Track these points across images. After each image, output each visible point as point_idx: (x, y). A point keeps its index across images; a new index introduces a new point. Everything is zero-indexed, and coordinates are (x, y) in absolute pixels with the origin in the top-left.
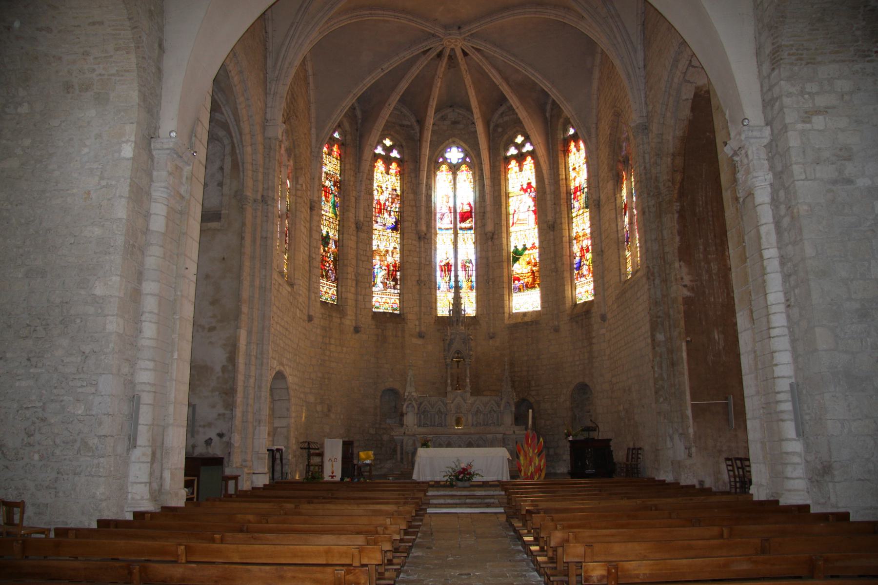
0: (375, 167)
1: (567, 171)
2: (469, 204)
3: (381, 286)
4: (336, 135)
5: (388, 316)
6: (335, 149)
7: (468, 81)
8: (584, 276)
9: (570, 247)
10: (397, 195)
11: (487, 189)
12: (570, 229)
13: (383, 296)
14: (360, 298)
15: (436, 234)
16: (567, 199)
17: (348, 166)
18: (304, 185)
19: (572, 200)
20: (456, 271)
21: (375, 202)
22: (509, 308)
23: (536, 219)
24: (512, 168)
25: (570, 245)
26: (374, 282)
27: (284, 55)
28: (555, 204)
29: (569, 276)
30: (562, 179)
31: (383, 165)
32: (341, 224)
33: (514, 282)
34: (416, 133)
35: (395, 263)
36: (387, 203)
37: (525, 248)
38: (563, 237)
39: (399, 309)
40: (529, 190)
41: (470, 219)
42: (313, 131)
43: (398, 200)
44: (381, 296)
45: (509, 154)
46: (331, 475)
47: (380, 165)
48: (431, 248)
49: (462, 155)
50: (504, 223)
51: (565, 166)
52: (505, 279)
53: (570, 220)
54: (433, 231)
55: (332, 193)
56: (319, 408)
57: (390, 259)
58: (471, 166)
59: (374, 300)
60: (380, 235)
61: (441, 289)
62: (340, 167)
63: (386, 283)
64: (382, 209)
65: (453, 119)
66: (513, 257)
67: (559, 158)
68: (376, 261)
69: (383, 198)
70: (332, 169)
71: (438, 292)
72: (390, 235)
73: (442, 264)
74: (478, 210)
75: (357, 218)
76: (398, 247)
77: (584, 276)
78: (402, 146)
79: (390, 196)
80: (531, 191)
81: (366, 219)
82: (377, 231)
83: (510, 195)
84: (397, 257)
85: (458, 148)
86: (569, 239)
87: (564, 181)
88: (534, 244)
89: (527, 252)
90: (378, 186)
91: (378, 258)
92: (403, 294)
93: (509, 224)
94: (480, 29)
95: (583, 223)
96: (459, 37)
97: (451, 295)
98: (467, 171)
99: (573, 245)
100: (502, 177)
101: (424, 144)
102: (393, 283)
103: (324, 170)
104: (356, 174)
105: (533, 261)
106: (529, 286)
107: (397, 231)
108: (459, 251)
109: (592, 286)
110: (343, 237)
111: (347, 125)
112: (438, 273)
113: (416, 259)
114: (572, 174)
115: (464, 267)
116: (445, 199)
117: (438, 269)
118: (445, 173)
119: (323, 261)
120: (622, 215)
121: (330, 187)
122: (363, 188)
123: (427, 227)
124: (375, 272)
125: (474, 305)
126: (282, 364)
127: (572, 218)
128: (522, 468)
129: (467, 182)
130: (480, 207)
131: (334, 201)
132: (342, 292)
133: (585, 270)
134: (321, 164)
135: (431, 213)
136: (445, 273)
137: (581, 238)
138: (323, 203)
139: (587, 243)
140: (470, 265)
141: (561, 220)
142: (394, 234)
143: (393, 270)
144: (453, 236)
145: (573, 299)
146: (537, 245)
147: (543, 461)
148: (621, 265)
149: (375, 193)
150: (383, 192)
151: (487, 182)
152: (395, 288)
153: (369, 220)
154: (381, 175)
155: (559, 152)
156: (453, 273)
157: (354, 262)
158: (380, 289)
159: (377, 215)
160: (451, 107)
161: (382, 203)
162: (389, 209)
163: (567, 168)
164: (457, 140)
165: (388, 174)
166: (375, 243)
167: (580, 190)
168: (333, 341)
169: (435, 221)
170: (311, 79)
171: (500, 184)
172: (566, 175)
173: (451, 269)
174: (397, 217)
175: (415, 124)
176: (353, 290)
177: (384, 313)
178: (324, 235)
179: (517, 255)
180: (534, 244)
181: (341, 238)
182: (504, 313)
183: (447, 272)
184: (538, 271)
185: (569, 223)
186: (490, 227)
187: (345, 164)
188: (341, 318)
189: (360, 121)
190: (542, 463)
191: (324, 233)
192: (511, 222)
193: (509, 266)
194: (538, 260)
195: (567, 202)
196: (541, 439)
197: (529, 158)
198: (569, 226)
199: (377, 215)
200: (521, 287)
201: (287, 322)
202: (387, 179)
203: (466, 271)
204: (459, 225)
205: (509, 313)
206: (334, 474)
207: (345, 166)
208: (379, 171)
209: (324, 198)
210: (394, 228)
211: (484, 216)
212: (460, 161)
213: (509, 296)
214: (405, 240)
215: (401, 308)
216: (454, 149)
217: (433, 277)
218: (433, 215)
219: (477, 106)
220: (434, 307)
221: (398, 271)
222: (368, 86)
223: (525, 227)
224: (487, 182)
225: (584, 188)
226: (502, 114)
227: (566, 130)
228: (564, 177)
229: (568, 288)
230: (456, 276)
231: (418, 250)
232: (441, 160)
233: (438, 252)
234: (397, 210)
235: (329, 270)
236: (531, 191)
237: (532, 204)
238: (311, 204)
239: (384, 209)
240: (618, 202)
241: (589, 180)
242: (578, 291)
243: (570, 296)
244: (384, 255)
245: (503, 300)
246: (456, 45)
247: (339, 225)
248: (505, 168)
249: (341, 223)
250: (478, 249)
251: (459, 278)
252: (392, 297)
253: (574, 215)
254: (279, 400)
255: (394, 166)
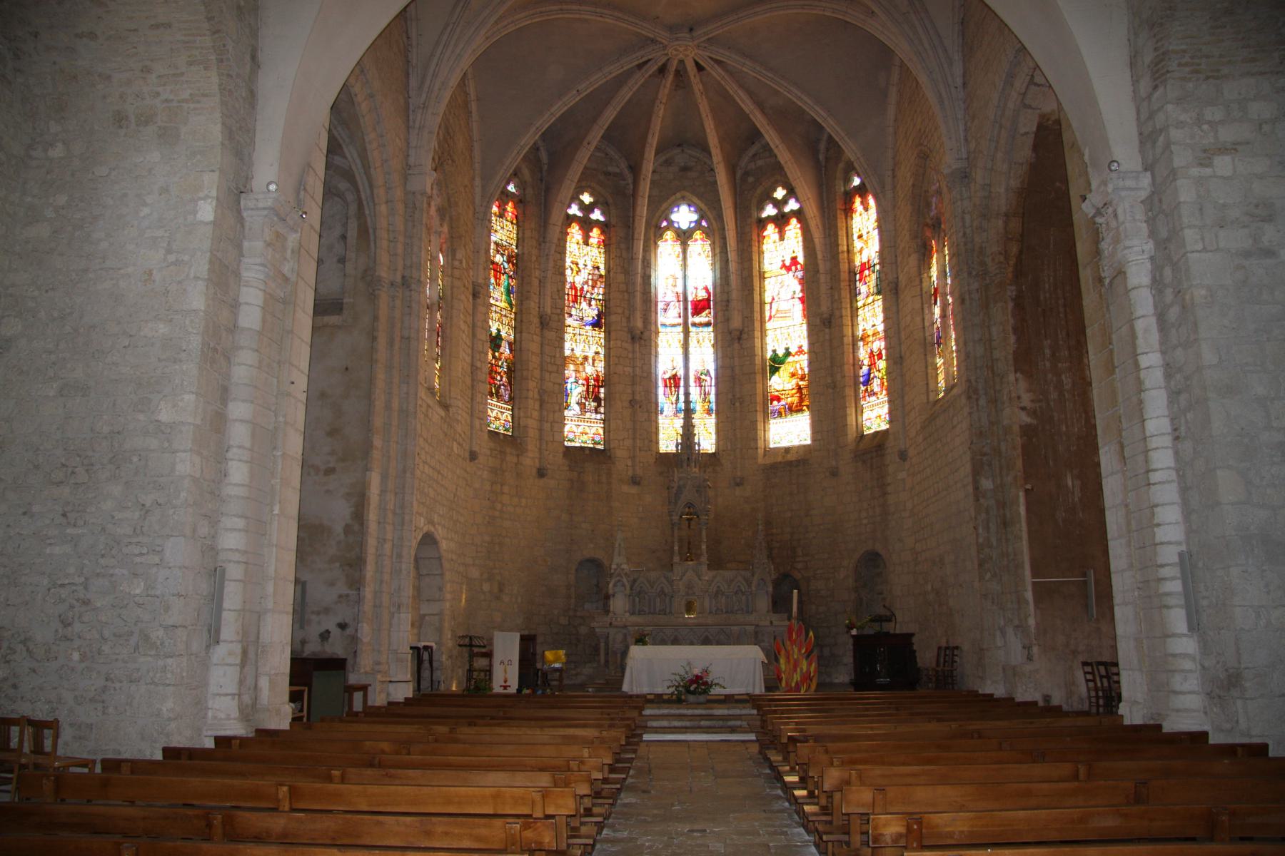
0: (568, 234)
1: (850, 241)
2: (706, 289)
3: (577, 408)
4: (511, 188)
5: (587, 452)
6: (510, 207)
7: (704, 108)
8: (875, 394)
9: (854, 352)
10: (601, 276)
11: (733, 266)
12: (854, 325)
13: (580, 423)
14: (547, 426)
15: (657, 333)
16: (850, 281)
17: (528, 233)
18: (464, 261)
19: (858, 283)
20: (687, 386)
21: (568, 286)
22: (765, 440)
23: (804, 310)
24: (769, 236)
25: (853, 349)
26: (566, 402)
27: (434, 71)
28: (831, 288)
29: (853, 394)
30: (843, 252)
31: (580, 232)
32: (518, 319)
33: (771, 404)
34: (628, 184)
35: (598, 376)
36: (586, 288)
37: (788, 354)
38: (843, 336)
39: (602, 443)
40: (793, 268)
41: (707, 311)
42: (478, 182)
43: (601, 282)
44: (576, 423)
45: (764, 215)
46: (504, 684)
47: (575, 232)
48: (650, 354)
49: (695, 217)
50: (757, 316)
51: (847, 233)
52: (759, 399)
53: (854, 312)
54: (653, 328)
55: (505, 273)
56: (486, 587)
57: (589, 370)
58: (708, 233)
59: (567, 429)
60: (575, 335)
61: (665, 413)
62: (517, 234)
63: (585, 404)
64: (578, 296)
65: (683, 164)
66: (771, 366)
67: (839, 220)
68: (570, 372)
69: (579, 280)
70: (504, 238)
71: (660, 417)
72: (590, 334)
73: (667, 376)
74: (718, 299)
75: (541, 309)
76: (602, 351)
77: (875, 394)
78: (607, 203)
79: (590, 277)
80: (796, 269)
81: (554, 311)
82: (571, 328)
83: (766, 275)
84: (600, 366)
85: (689, 206)
86: (853, 340)
87: (846, 255)
88: (800, 347)
89: (790, 359)
90: (572, 263)
91: (572, 367)
92: (609, 420)
93: (765, 317)
94: (721, 31)
95: (873, 316)
96: (691, 44)
97: (679, 423)
98: (702, 239)
99: (858, 349)
100: (755, 249)
101: (639, 201)
102: (593, 404)
103: (493, 238)
104: (540, 245)
105: (800, 372)
106: (793, 409)
107: (601, 328)
108: (692, 357)
109: (886, 409)
110: (521, 338)
111: (526, 173)
112: (661, 390)
113: (628, 369)
114: (858, 244)
115: (699, 380)
116: (671, 281)
117: (661, 384)
118: (670, 242)
119: (492, 372)
120: (930, 305)
121: (502, 264)
122: (551, 264)
123: (644, 322)
124: (569, 388)
125: (714, 437)
126: (431, 522)
127: (857, 309)
128: (783, 675)
129: (703, 256)
130: (722, 292)
131: (509, 284)
132: (519, 418)
133: (876, 385)
134: (489, 230)
135: (650, 301)
136: (671, 389)
137: (871, 339)
138: (491, 287)
139: (879, 345)
140: (708, 378)
141: (841, 313)
142: (596, 333)
143: (594, 385)
144: (682, 335)
145: (859, 427)
146: (805, 348)
147: (813, 665)
148: (929, 378)
149: (568, 272)
150: (580, 271)
151: (732, 256)
152: (597, 412)
153: (559, 311)
154: (576, 247)
155: (839, 212)
156: (682, 390)
157: (537, 373)
158: (575, 413)
159: (571, 304)
160: (679, 145)
161: (579, 286)
162: (588, 296)
163: (850, 235)
164: (687, 194)
165: (587, 245)
166: (567, 345)
167: (869, 268)
168: (506, 489)
169: (656, 313)
170: (474, 106)
171: (751, 260)
172: (848, 246)
173: (679, 383)
174: (600, 307)
175: (626, 172)
176: (536, 414)
177: (582, 448)
178: (494, 334)
179: (776, 363)
180: (800, 347)
181: (518, 339)
182: (757, 448)
183: (673, 389)
184: (807, 387)
185: (852, 317)
186: (736, 323)
187: (523, 230)
188: (518, 456)
189: (546, 167)
190: (812, 669)
191: (494, 331)
192: (767, 314)
193: (765, 380)
194: (806, 371)
195: (850, 285)
196: (811, 634)
197: (794, 221)
198: (852, 320)
199: (571, 304)
200: (783, 410)
201: (440, 462)
202: (585, 252)
203: (701, 386)
204: (691, 320)
205: (765, 449)
206: (508, 684)
207: (523, 233)
208: (574, 240)
209: (493, 280)
210: (596, 324)
211: (727, 306)
212: (693, 225)
213: (764, 422)
214: (612, 342)
215: (607, 441)
216: (684, 209)
217: (653, 396)
218: (653, 305)
219: (718, 145)
220: (654, 440)
221: (602, 387)
222: (557, 116)
223: (789, 322)
224: (732, 256)
225: (875, 265)
226: (754, 155)
227: (848, 180)
228: (845, 248)
229: (851, 411)
230: (687, 394)
231: (630, 356)
232: (664, 224)
233: (661, 359)
234: (600, 297)
235: (500, 385)
236: (796, 269)
237: (798, 288)
238: (474, 289)
239: (581, 296)
240: (925, 285)
241: (881, 253)
242: (865, 416)
243: (854, 423)
244: (582, 364)
245: (756, 429)
246: (687, 56)
247: (515, 320)
248: (758, 235)
249: (518, 316)
250: (720, 355)
251: (691, 396)
252: (592, 425)
253: (860, 304)
254: (428, 575)
255: (595, 232)
